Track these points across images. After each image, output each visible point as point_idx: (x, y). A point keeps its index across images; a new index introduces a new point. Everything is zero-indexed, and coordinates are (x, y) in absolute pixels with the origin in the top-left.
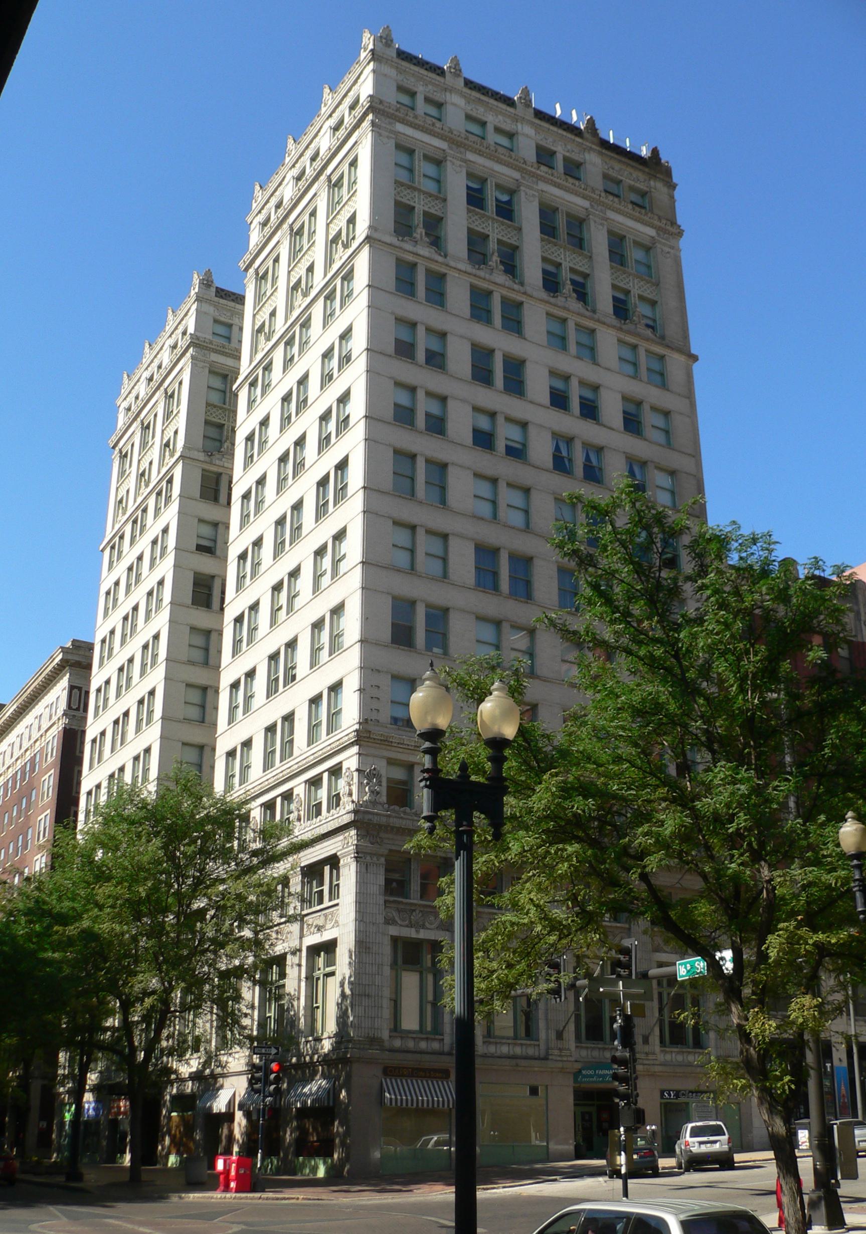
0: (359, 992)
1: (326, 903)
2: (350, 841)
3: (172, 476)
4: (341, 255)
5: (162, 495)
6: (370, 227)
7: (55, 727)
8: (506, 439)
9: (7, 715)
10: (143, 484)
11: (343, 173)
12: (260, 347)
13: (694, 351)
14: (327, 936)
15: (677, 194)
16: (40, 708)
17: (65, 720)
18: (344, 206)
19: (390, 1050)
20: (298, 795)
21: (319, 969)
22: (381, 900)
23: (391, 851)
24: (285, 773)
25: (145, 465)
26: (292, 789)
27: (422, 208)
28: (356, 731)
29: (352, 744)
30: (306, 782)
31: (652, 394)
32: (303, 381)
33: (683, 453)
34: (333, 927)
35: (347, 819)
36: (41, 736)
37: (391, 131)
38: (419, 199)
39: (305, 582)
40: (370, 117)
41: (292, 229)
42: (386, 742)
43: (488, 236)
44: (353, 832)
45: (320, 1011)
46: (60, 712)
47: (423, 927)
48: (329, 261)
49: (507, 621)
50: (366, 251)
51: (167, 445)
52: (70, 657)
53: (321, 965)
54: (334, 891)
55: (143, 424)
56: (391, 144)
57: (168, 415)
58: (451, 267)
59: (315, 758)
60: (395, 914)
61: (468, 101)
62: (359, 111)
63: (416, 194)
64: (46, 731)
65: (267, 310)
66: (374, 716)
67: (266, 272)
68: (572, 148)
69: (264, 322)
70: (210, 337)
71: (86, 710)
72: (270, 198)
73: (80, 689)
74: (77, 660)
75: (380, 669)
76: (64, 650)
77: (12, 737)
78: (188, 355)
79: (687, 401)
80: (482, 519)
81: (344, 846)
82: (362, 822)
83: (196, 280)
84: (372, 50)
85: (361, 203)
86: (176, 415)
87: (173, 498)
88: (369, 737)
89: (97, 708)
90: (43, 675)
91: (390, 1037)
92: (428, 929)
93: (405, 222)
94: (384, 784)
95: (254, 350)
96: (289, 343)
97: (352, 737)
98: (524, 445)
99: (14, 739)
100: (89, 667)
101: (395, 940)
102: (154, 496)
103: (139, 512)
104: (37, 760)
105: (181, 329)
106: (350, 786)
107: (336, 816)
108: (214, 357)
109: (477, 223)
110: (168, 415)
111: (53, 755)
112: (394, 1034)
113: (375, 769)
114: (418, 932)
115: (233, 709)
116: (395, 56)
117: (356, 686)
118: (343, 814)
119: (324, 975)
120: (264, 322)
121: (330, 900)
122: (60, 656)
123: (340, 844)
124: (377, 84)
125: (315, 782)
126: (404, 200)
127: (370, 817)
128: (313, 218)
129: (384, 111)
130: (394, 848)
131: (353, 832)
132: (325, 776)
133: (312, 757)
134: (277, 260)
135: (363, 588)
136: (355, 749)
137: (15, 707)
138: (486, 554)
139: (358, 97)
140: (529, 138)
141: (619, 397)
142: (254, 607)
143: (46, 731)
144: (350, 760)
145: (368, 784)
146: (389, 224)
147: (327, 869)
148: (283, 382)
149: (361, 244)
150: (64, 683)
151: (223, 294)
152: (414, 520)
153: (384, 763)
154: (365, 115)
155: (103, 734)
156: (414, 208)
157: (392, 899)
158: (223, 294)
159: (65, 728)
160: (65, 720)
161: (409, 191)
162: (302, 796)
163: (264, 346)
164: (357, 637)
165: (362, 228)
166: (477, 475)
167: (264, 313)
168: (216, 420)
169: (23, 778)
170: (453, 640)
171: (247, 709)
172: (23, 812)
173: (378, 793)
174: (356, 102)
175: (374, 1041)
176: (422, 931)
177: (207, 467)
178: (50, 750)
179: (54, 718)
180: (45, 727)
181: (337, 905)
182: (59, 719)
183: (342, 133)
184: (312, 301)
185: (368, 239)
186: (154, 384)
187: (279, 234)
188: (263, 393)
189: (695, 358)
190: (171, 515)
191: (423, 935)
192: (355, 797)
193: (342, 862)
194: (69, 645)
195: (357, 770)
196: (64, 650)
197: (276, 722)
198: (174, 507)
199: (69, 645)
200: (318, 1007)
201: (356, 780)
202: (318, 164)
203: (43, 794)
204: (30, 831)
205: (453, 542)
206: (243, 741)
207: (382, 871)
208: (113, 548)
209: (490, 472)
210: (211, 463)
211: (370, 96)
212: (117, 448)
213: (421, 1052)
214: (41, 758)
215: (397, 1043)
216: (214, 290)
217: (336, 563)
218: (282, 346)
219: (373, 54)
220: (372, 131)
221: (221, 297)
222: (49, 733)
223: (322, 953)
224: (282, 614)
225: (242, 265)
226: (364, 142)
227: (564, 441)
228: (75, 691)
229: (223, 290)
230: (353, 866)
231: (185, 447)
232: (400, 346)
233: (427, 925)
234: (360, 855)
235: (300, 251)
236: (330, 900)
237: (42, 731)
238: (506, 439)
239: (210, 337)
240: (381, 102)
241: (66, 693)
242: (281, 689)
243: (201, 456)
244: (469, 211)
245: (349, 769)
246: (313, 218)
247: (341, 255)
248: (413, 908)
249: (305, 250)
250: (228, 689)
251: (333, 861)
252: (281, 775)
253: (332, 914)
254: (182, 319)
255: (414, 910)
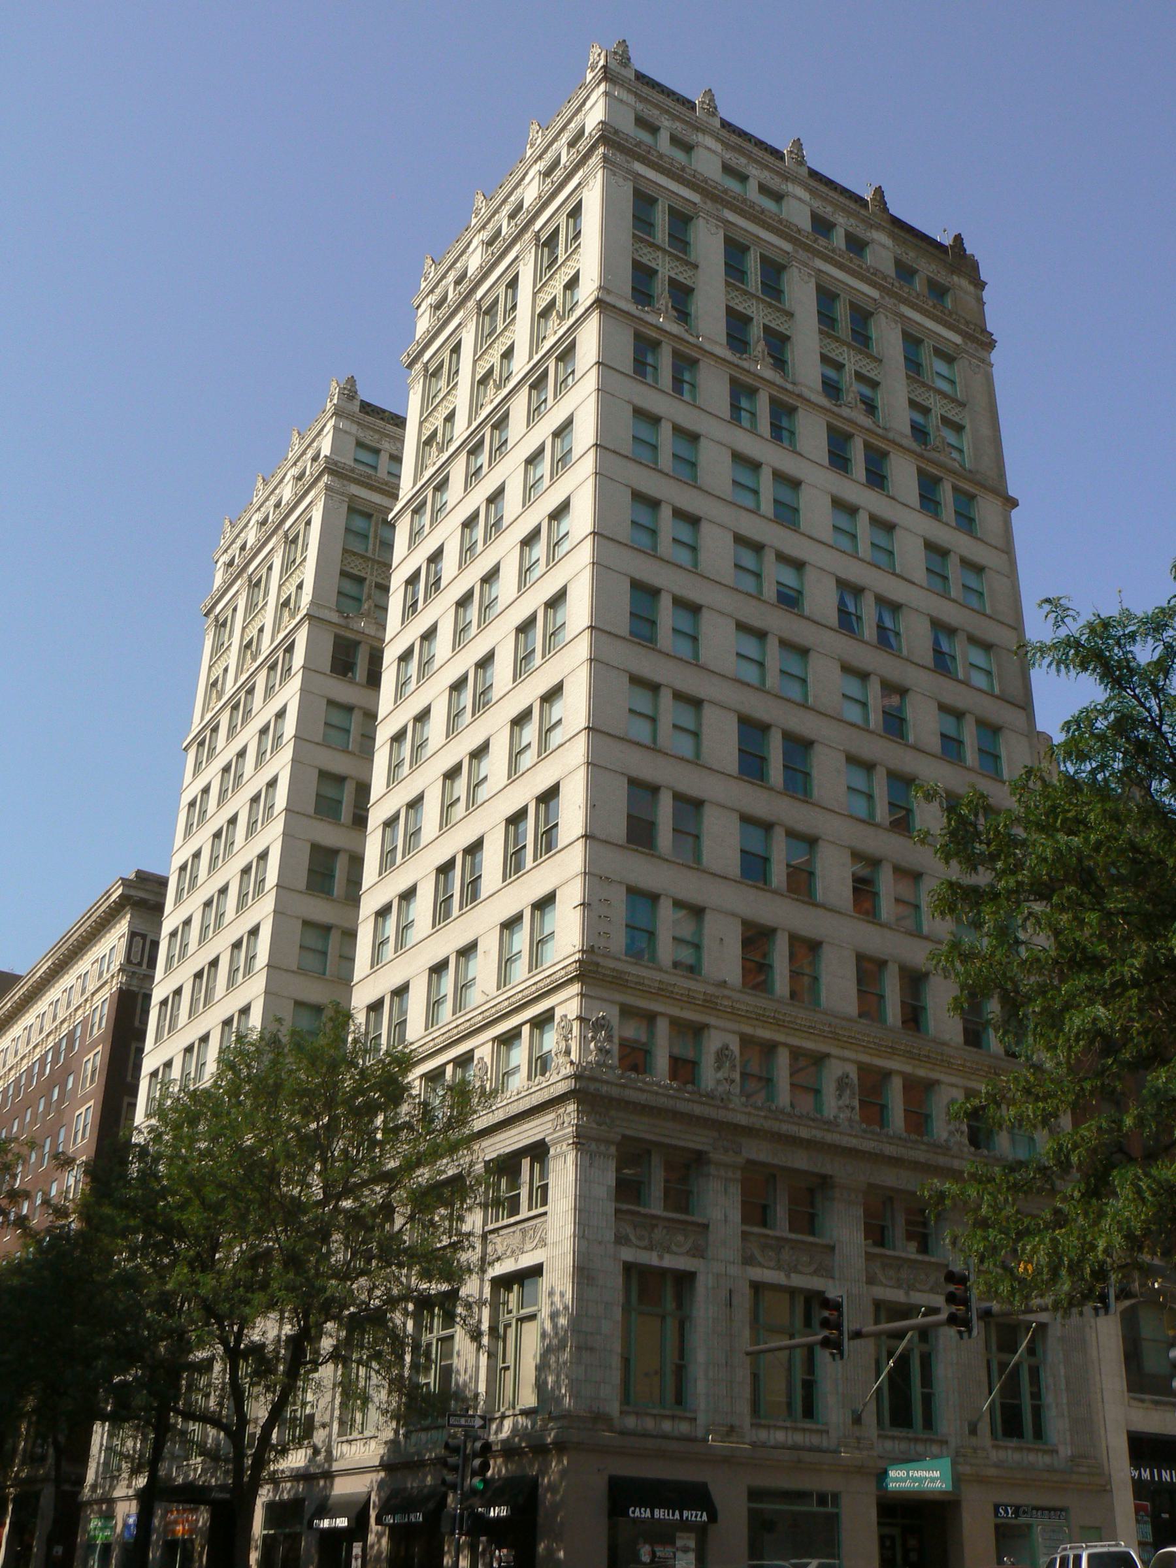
0: (577, 1338)
1: (524, 1213)
2: (567, 1119)
3: (294, 641)
4: (492, 398)
5: (276, 667)
6: (600, 288)
7: (107, 987)
8: (778, 583)
9: (38, 975)
10: (249, 656)
11: (498, 297)
12: (283, 625)
13: (1012, 493)
14: (526, 1261)
15: (986, 295)
16: (84, 965)
17: (122, 978)
18: (560, 267)
19: (622, 1433)
20: (482, 1059)
21: (510, 1312)
22: (610, 1207)
23: (624, 1136)
24: (462, 1027)
25: (218, 671)
26: (472, 1050)
27: (667, 274)
28: (579, 961)
29: (570, 981)
30: (494, 1039)
31: (960, 543)
32: (436, 557)
33: (1002, 623)
34: (535, 1248)
35: (562, 1088)
36: (86, 1000)
37: (629, 171)
38: (664, 261)
39: (496, 764)
40: (601, 150)
41: (479, 307)
42: (617, 981)
43: (752, 319)
44: (572, 1107)
45: (510, 1374)
46: (115, 967)
47: (668, 1250)
48: (475, 406)
49: (781, 825)
50: (595, 318)
51: (248, 646)
52: (133, 892)
53: (513, 1305)
54: (542, 1194)
55: (426, 370)
56: (628, 188)
57: (289, 565)
58: (706, 351)
59: (484, 1019)
60: (629, 1230)
61: (726, 145)
62: (583, 145)
63: (659, 254)
64: (93, 994)
65: (256, 625)
66: (602, 943)
67: (297, 536)
68: (851, 219)
69: (290, 595)
70: (352, 463)
71: (152, 964)
72: (306, 449)
73: (144, 937)
74: (144, 897)
75: (612, 876)
76: (125, 882)
77: (16, 1030)
78: (321, 484)
79: (1005, 556)
80: (748, 685)
81: (558, 1128)
82: (586, 1092)
83: (334, 389)
84: (603, 66)
85: (589, 261)
86: (262, 608)
87: (293, 672)
88: (596, 972)
89: (169, 959)
90: (93, 918)
91: (621, 1413)
92: (676, 1253)
93: (644, 292)
94: (616, 1040)
95: (420, 467)
96: (475, 451)
97: (572, 970)
98: (800, 593)
99: (59, 995)
100: (159, 908)
101: (628, 1268)
102: (264, 671)
103: (208, 732)
104: (78, 1034)
105: (239, 543)
106: (567, 1041)
107: (544, 1085)
108: (355, 490)
109: (737, 301)
110: (289, 565)
111: (101, 1026)
112: (625, 1408)
113: (603, 1017)
114: (661, 1257)
115: (379, 945)
116: (633, 78)
117: (578, 898)
118: (558, 1081)
119: (517, 1320)
120: (290, 595)
121: (530, 1209)
122: (120, 891)
123: (549, 1125)
124: (609, 109)
125: (508, 1040)
126: (644, 260)
127: (598, 1085)
128: (454, 356)
129: (619, 144)
130: (629, 1132)
131: (572, 1107)
132: (526, 1029)
133: (506, 1003)
134: (308, 523)
135: (588, 763)
136: (575, 988)
137: (49, 963)
138: (752, 729)
139: (522, 201)
140: (798, 210)
141: (921, 542)
142: (416, 804)
143: (93, 994)
144: (568, 1004)
145: (593, 1038)
146: (625, 285)
147: (526, 1163)
148: (462, 500)
149: (587, 310)
150: (122, 927)
151: (369, 409)
152: (657, 678)
153: (616, 1011)
154: (593, 148)
155: (178, 992)
156: (656, 272)
157: (625, 1207)
158: (369, 409)
159: (120, 990)
160: (122, 978)
161: (649, 249)
162: (488, 1060)
163: (436, 459)
164: (579, 830)
165: (587, 291)
166: (742, 627)
167: (437, 419)
168: (355, 572)
169: (55, 1060)
170: (707, 843)
171: (400, 943)
172: (54, 1106)
173: (608, 1052)
174: (581, 133)
175: (599, 1418)
176: (667, 1256)
177: (342, 632)
178: (97, 1019)
179: (106, 976)
180: (91, 988)
181: (545, 1214)
182: (113, 976)
183: (444, 311)
184: (510, 392)
185: (599, 303)
186: (270, 526)
187: (274, 540)
188: (434, 519)
189: (1014, 503)
190: (290, 693)
191: (669, 1262)
192: (574, 1056)
193: (552, 1152)
194: (132, 876)
195: (579, 1018)
196: (125, 882)
197: (448, 958)
198: (295, 683)
199: (132, 876)
200: (508, 1368)
201: (576, 1031)
202: (464, 287)
203: (85, 1078)
204: (63, 1131)
205: (708, 711)
206: (394, 987)
207: (612, 1165)
208: (201, 744)
209: (757, 623)
210: (347, 627)
211: (601, 122)
212: (212, 616)
213: (665, 1437)
214: (83, 1032)
215: (631, 1422)
216: (358, 403)
217: (545, 733)
218: (463, 456)
219: (605, 72)
220: (604, 167)
221: (367, 413)
222: (96, 998)
223: (516, 1287)
224: (460, 810)
225: (405, 359)
226: (591, 184)
227: (849, 589)
228: (138, 938)
229: (369, 405)
230: (571, 1157)
231: (312, 603)
232: (638, 443)
233: (674, 1248)
234: (581, 1141)
235: (490, 335)
236: (530, 1209)
237: (72, 1009)
238: (778, 583)
239: (352, 463)
240: (616, 132)
241: (124, 941)
242: (455, 912)
243: (334, 617)
244: (727, 284)
245: (566, 1016)
246: (454, 356)
247: (492, 398)
248: (654, 1222)
249: (559, 262)
250: (372, 919)
251: (538, 1151)
252: (455, 1031)
253: (535, 1228)
254: (313, 441)
255: (656, 1226)
